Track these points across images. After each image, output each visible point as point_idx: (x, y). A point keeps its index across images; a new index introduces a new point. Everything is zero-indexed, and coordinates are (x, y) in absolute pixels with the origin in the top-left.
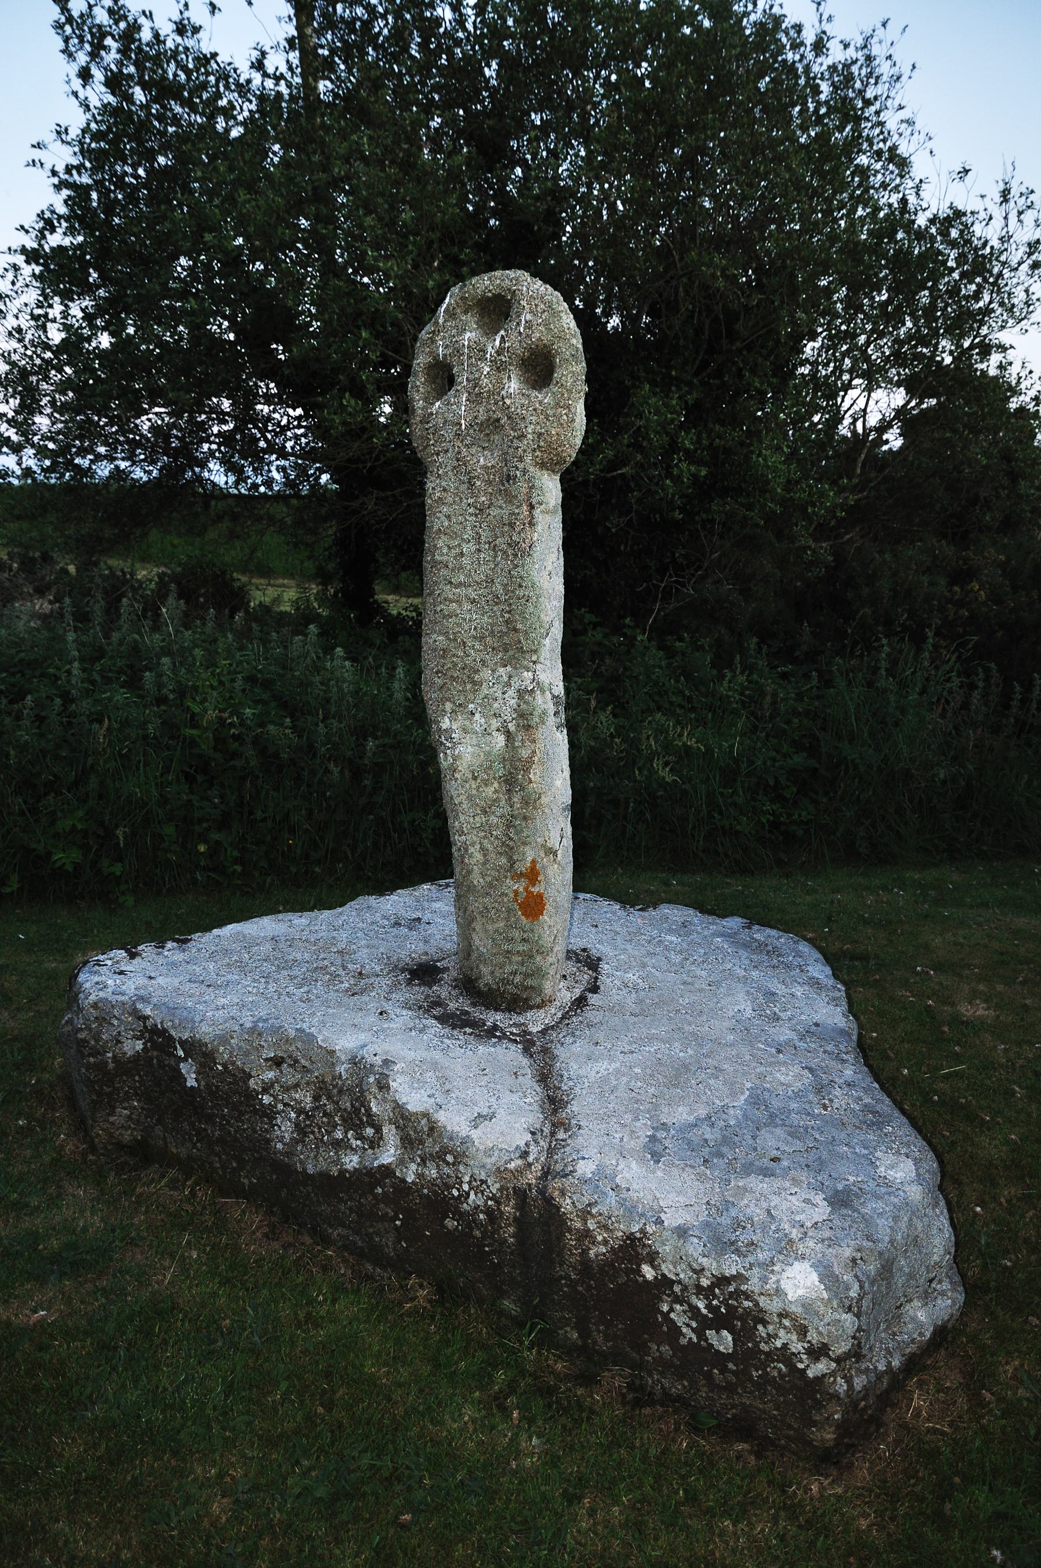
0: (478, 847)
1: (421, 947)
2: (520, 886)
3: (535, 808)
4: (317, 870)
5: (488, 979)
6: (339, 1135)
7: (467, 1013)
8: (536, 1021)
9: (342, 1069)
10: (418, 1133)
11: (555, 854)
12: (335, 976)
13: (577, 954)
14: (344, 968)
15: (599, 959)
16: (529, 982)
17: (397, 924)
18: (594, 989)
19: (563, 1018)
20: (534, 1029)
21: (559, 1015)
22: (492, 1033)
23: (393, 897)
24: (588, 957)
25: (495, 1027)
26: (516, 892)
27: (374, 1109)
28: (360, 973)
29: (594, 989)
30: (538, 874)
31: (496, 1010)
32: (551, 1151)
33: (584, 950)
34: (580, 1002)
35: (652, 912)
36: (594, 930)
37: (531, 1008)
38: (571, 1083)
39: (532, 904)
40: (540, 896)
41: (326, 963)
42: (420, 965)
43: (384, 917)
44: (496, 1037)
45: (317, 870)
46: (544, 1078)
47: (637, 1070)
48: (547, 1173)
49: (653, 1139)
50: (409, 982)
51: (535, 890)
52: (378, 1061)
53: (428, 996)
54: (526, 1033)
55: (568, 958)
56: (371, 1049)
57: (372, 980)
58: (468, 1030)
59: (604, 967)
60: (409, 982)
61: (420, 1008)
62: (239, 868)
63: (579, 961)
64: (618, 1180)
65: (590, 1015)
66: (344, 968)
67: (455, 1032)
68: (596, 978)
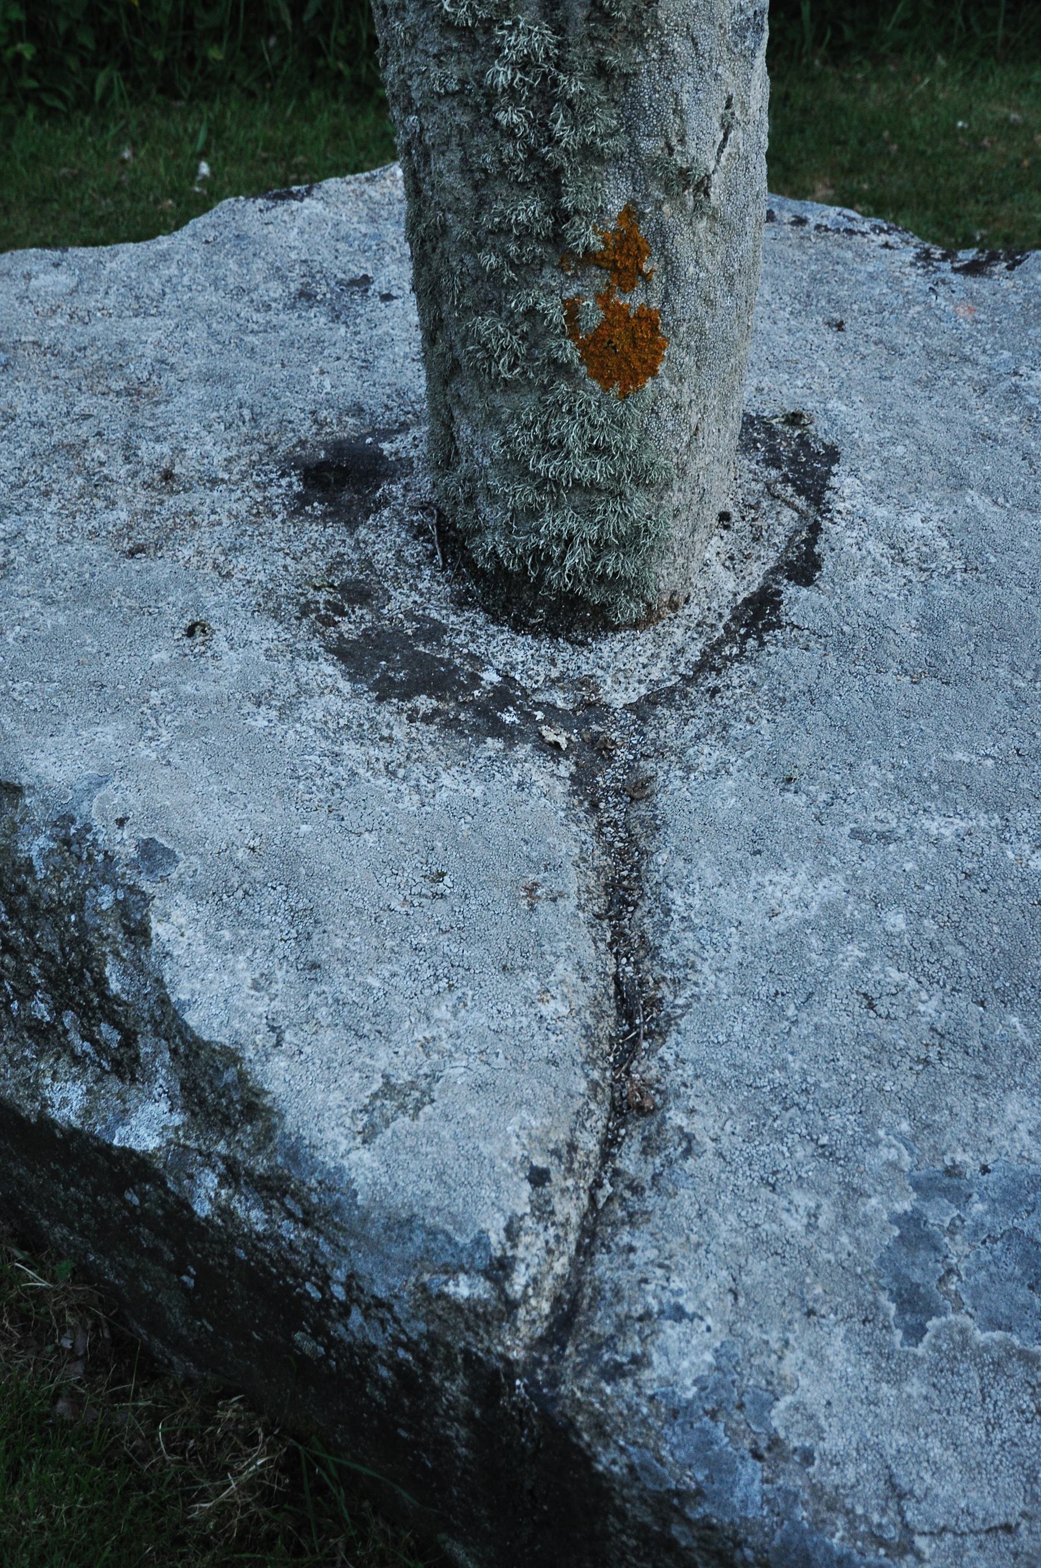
0: (455, 156)
1: (350, 385)
2: (586, 290)
3: (637, 38)
4: (216, 54)
5: (492, 541)
6: (41, 1010)
7: (435, 632)
8: (624, 667)
9: (36, 846)
10: (219, 1092)
11: (703, 187)
12: (97, 483)
13: (771, 432)
14: (129, 452)
15: (832, 455)
16: (611, 564)
17: (306, 295)
18: (803, 568)
19: (702, 666)
20: (618, 697)
21: (694, 653)
22: (491, 715)
23: (311, 206)
24: (803, 442)
25: (505, 694)
26: (572, 309)
27: (115, 986)
28: (168, 476)
29: (803, 568)
30: (640, 254)
31: (519, 626)
32: (591, 1237)
33: (794, 419)
34: (759, 613)
35: (1003, 283)
36: (831, 337)
37: (616, 629)
38: (689, 941)
39: (623, 344)
40: (648, 319)
41: (85, 430)
42: (338, 448)
43: (278, 274)
44: (498, 729)
45: (216, 54)
46: (622, 896)
47: (896, 920)
48: (566, 1319)
49: (913, 1232)
50: (298, 507)
51: (634, 300)
52: (124, 845)
53: (338, 563)
54: (593, 709)
55: (747, 446)
56: (118, 796)
57: (195, 498)
58: (424, 703)
59: (846, 487)
60: (298, 507)
61: (304, 611)
62: (27, 50)
63: (773, 461)
64: (778, 1417)
65: (782, 657)
66: (129, 452)
67: (386, 713)
68: (815, 529)
